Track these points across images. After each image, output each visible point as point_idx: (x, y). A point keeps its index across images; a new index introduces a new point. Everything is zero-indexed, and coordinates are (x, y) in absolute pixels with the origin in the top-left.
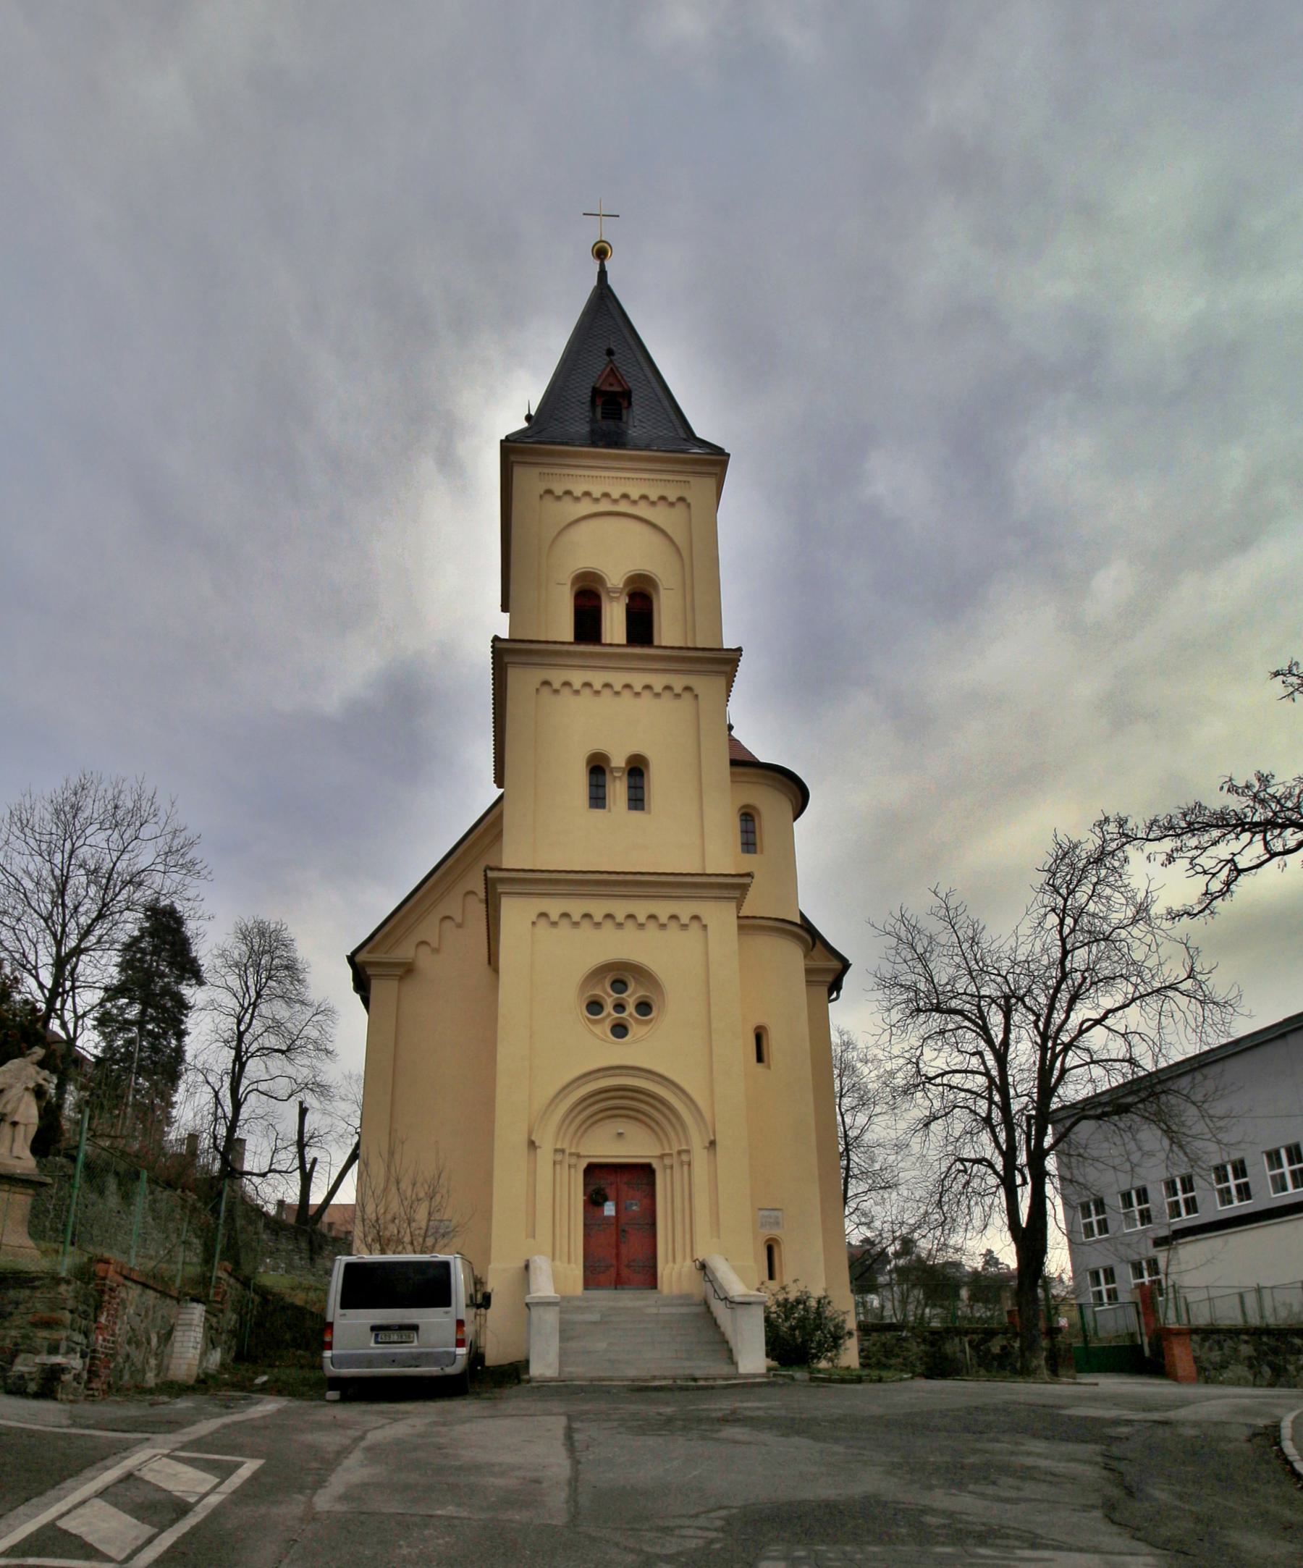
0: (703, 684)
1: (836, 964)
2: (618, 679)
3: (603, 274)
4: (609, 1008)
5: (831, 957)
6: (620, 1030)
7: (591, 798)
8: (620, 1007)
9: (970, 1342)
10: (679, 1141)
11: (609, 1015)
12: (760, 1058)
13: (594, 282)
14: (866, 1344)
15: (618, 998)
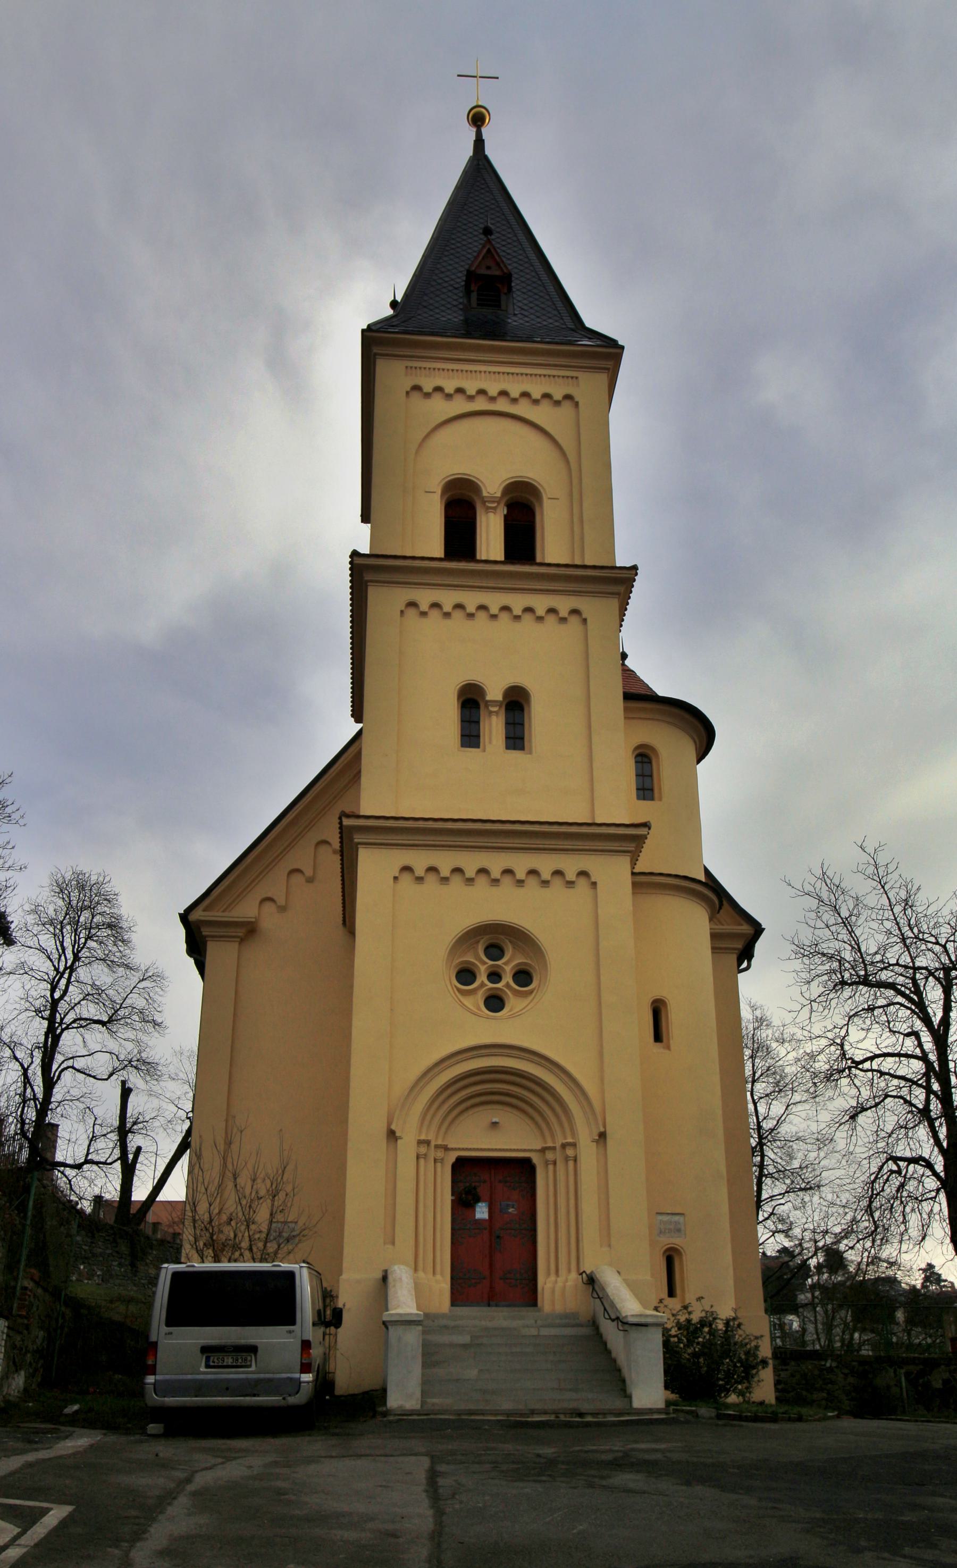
1: (746, 929)
2: (495, 601)
3: (479, 143)
4: (482, 978)
5: (742, 922)
8: (495, 976)
9: (907, 1375)
11: (483, 985)
12: (658, 1037)
13: (469, 152)
14: (783, 1374)
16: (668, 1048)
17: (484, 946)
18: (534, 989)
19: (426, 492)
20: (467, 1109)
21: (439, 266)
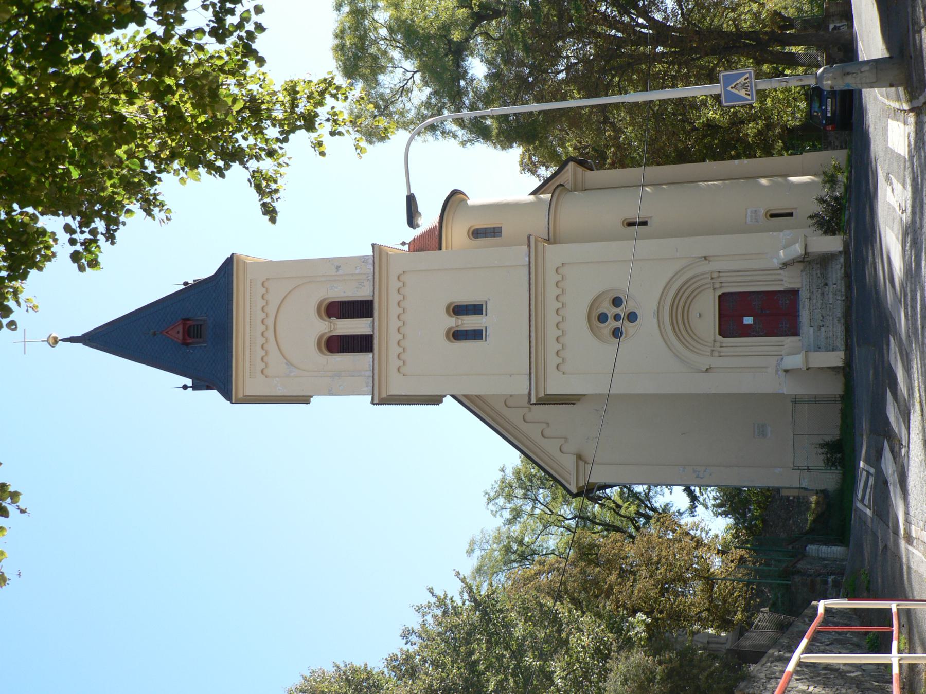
4: (618, 324)
6: (632, 317)
8: (617, 317)
10: (706, 278)
13: (80, 346)
15: (611, 318)
16: (651, 217)
20: (698, 338)
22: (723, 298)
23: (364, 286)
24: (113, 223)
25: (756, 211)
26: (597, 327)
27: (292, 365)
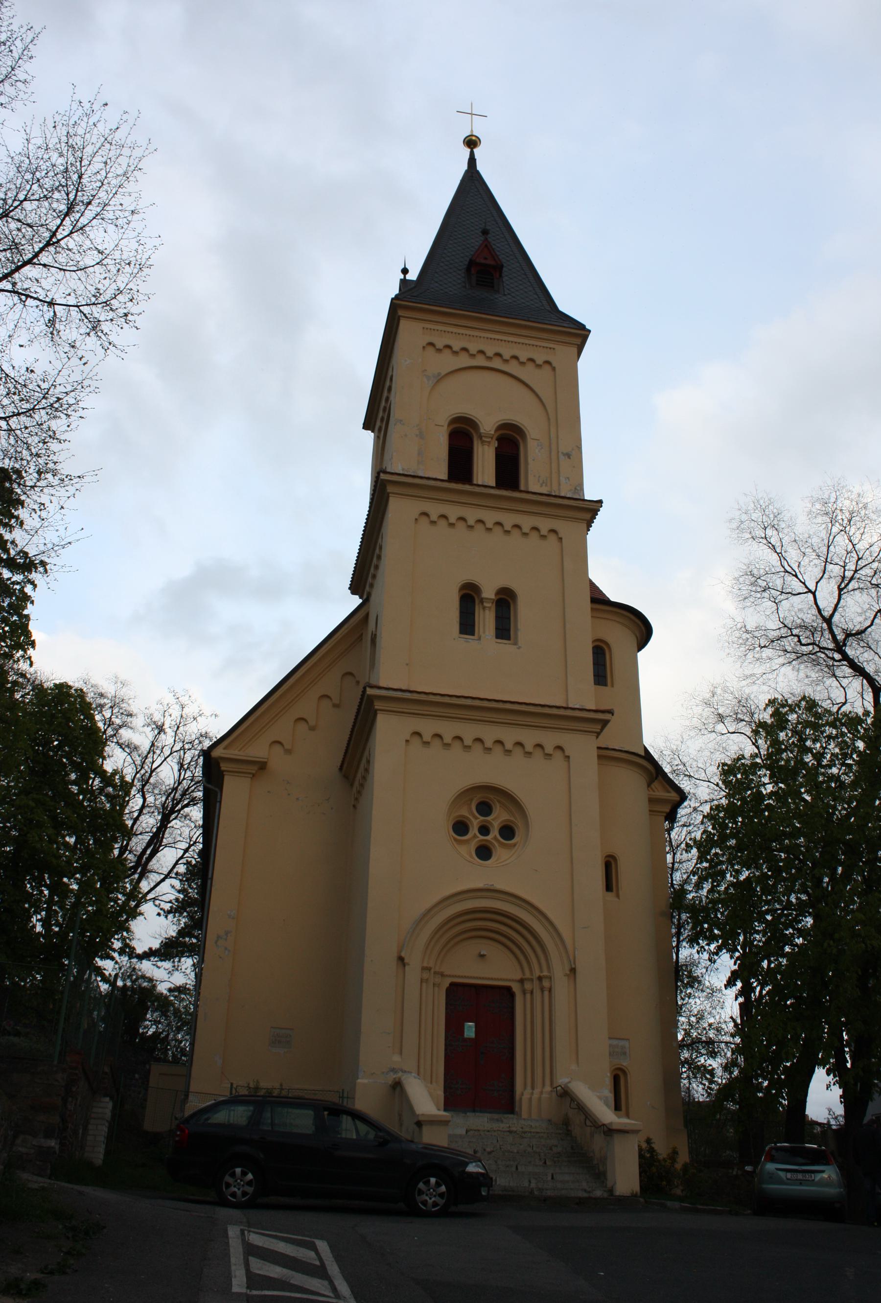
0: (564, 527)
1: (674, 796)
2: (490, 517)
3: (472, 161)
4: (474, 830)
5: (670, 789)
7: (461, 624)
8: (484, 830)
11: (475, 836)
12: (609, 888)
15: (483, 821)
17: (478, 801)
18: (517, 842)
19: (436, 425)
21: (445, 251)
22: (507, 993)
23: (541, 486)
24: (128, 930)
25: (625, 1053)
26: (472, 800)
27: (438, 381)
